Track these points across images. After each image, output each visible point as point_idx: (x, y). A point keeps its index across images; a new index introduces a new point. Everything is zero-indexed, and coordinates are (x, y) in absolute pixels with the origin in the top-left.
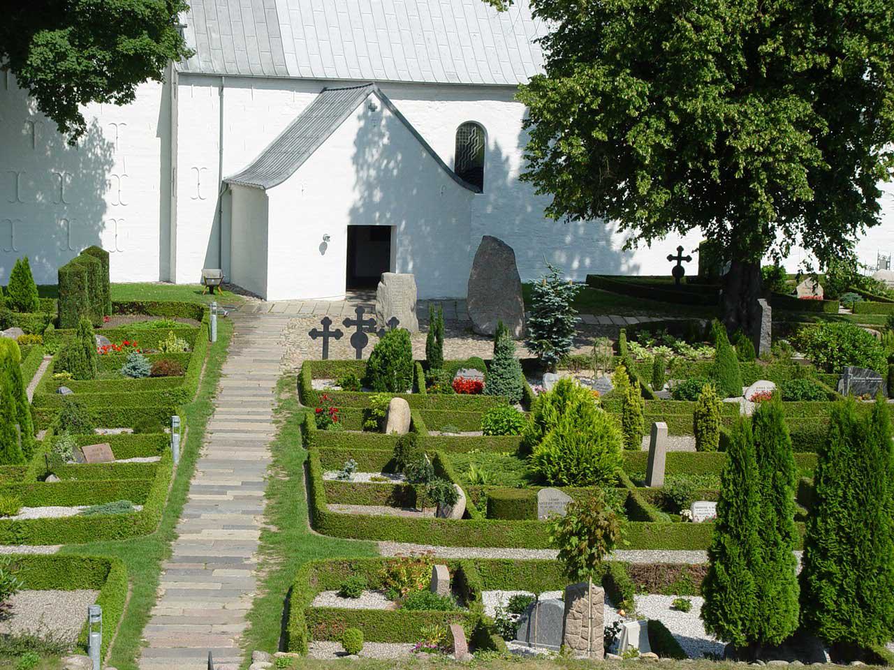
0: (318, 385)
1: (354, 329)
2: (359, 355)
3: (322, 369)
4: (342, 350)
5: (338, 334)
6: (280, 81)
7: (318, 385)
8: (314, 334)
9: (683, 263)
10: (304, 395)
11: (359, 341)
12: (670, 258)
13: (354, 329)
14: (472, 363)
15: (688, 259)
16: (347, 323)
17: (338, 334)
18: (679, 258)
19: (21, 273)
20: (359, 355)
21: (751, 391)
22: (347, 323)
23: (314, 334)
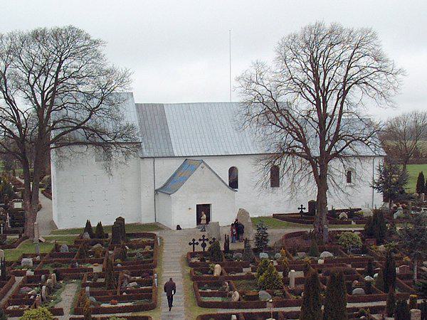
0: (194, 260)
1: (202, 242)
2: (204, 249)
3: (193, 255)
4: (199, 248)
5: (197, 244)
6: (224, 159)
7: (194, 260)
8: (190, 244)
9: (205, 242)
10: (191, 265)
11: (204, 245)
12: (299, 209)
13: (202, 242)
14: (239, 251)
15: (305, 208)
16: (200, 240)
17: (197, 244)
18: (302, 209)
19: (88, 223)
20: (204, 249)
21: (322, 255)
22: (200, 240)
23: (190, 244)
